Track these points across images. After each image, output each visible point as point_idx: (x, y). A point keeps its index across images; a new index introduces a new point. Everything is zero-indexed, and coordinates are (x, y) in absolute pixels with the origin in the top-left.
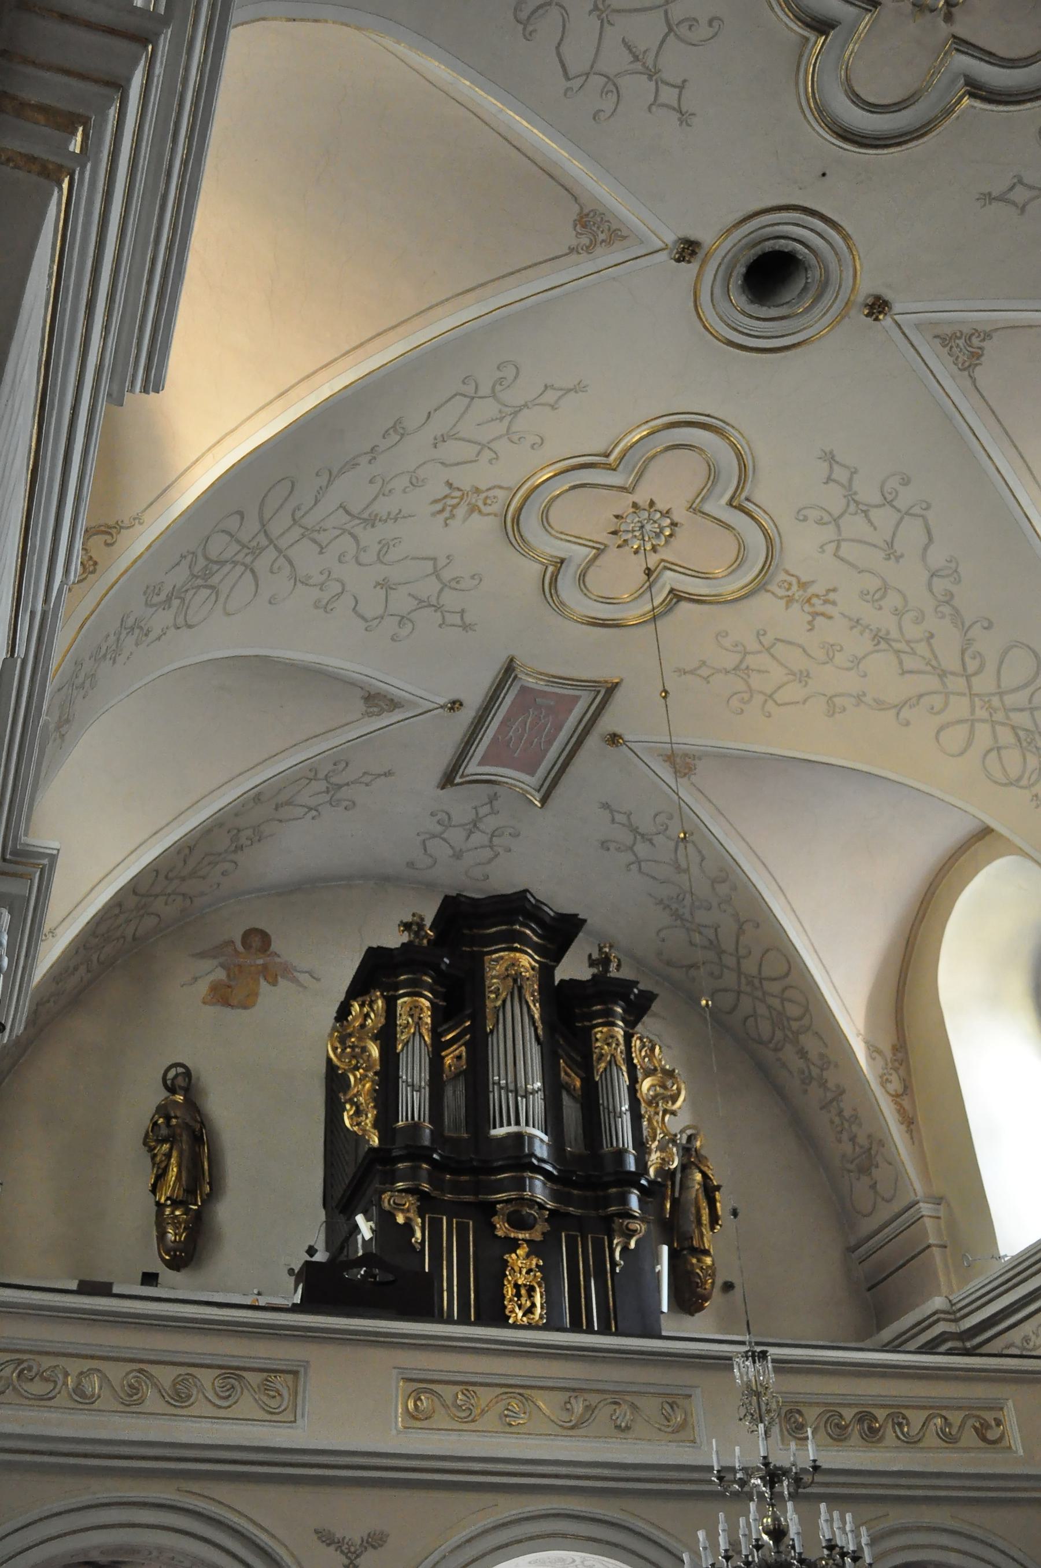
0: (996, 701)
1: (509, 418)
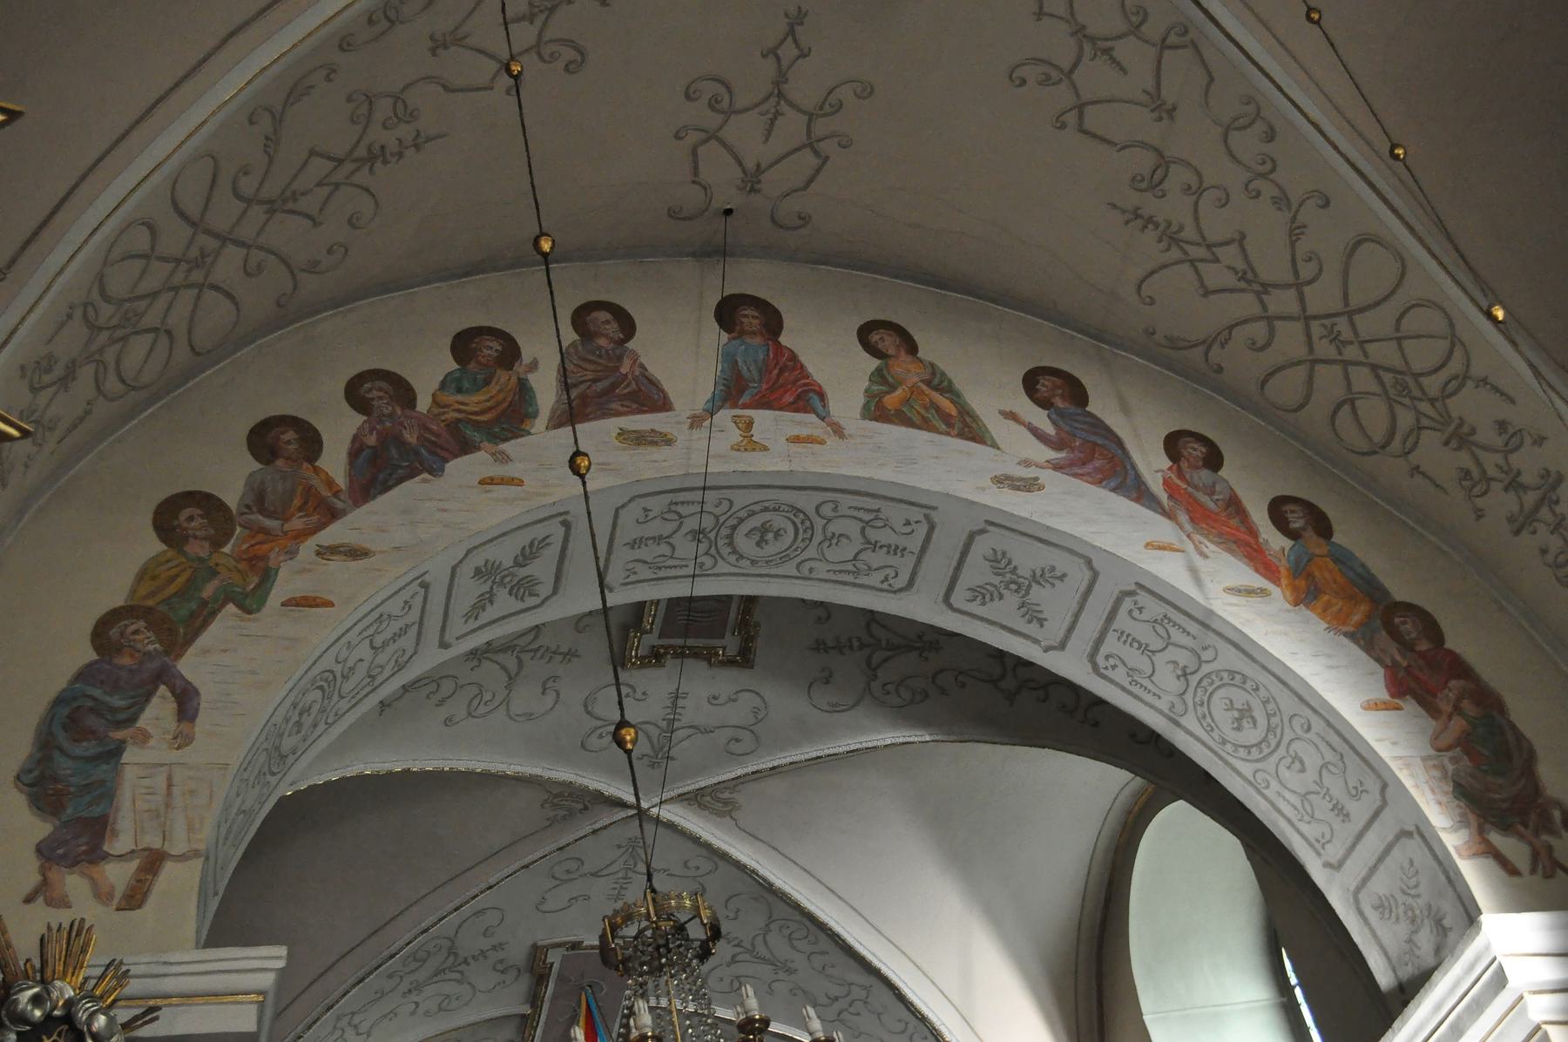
0: (1342, 325)
1: (543, 17)
